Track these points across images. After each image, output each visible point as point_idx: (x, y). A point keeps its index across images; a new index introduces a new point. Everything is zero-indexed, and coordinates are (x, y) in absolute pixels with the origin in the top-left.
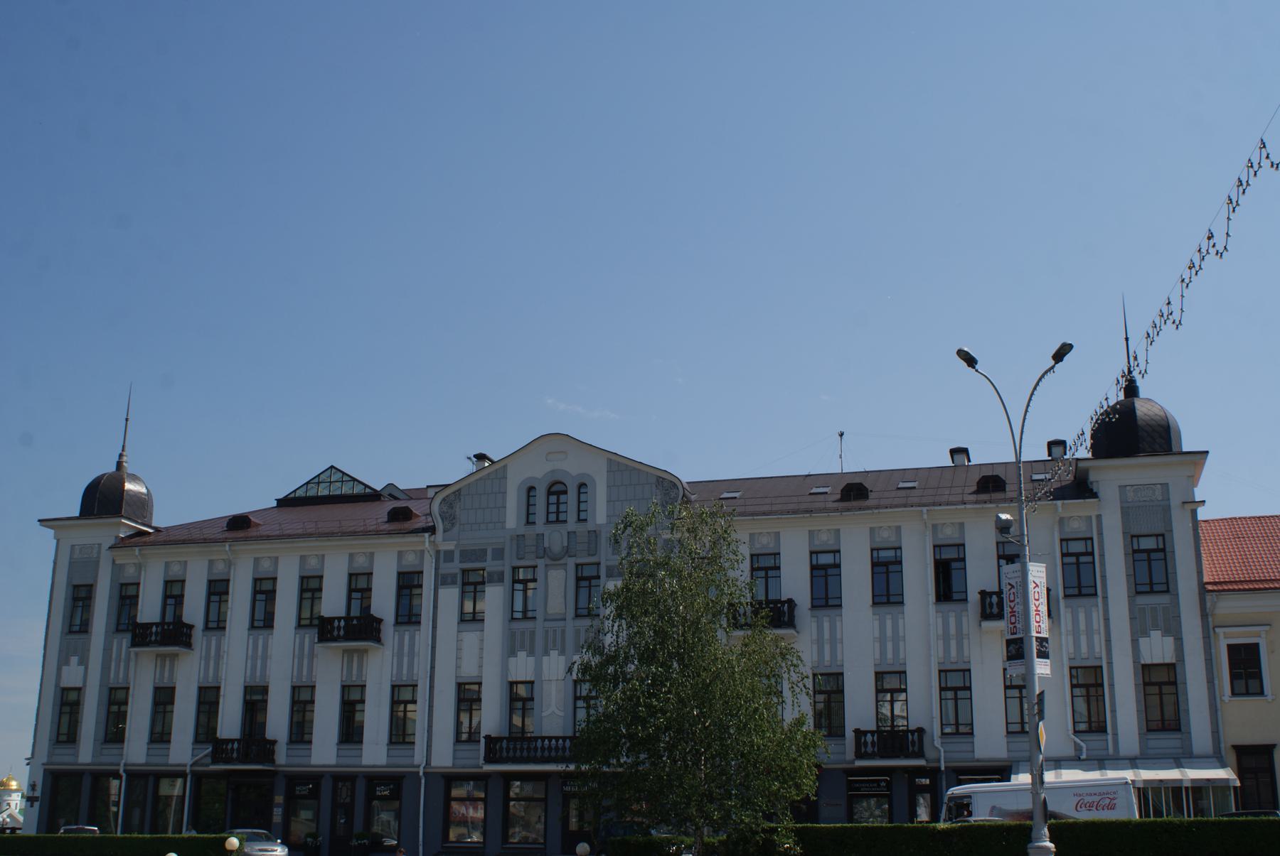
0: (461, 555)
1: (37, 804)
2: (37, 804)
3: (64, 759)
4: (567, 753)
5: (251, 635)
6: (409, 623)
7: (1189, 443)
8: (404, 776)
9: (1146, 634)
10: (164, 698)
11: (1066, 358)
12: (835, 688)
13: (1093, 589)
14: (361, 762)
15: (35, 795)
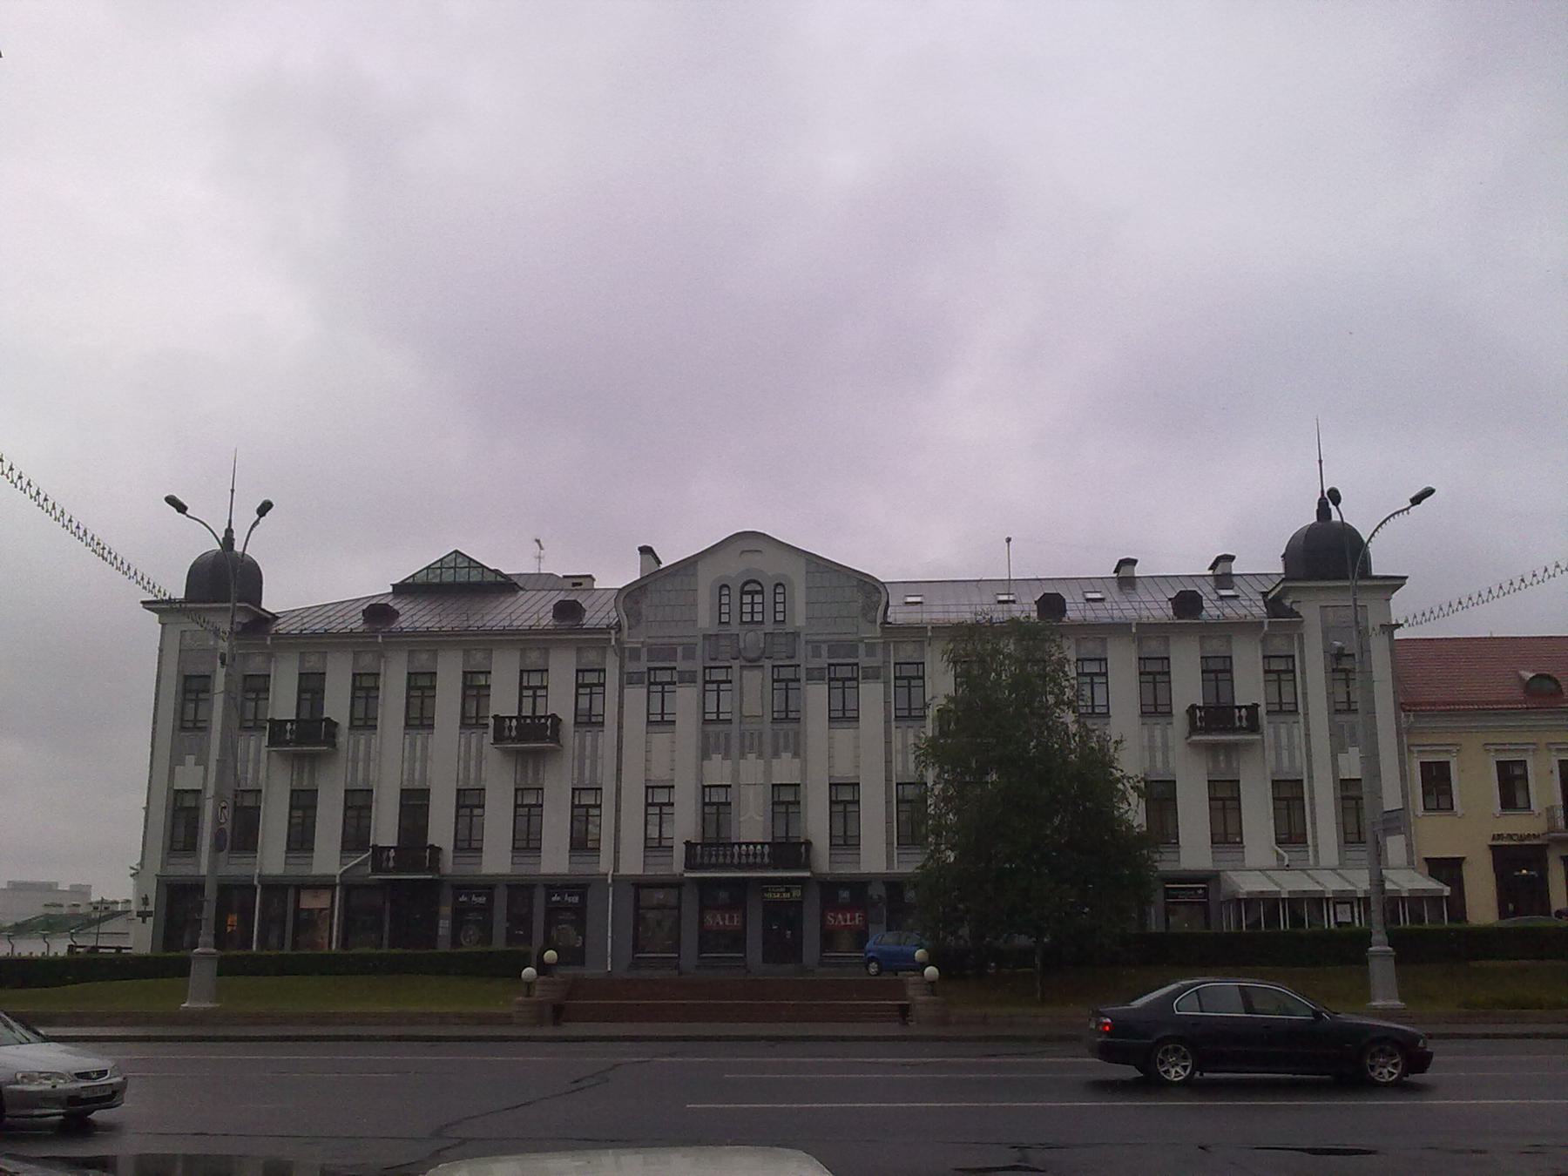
0: (650, 652)
1: (150, 920)
2: (150, 920)
3: (182, 869)
4: (766, 860)
5: (463, 733)
6: (422, 726)
7: (1380, 565)
8: (870, 882)
9: (1343, 749)
10: (303, 803)
11: (267, 514)
12: (724, 800)
13: (856, 712)
14: (199, 871)
15: (147, 910)
